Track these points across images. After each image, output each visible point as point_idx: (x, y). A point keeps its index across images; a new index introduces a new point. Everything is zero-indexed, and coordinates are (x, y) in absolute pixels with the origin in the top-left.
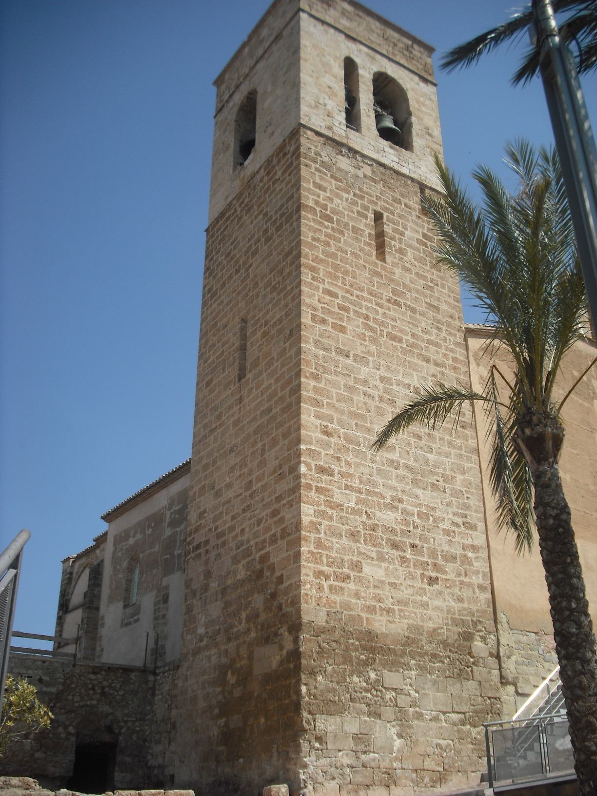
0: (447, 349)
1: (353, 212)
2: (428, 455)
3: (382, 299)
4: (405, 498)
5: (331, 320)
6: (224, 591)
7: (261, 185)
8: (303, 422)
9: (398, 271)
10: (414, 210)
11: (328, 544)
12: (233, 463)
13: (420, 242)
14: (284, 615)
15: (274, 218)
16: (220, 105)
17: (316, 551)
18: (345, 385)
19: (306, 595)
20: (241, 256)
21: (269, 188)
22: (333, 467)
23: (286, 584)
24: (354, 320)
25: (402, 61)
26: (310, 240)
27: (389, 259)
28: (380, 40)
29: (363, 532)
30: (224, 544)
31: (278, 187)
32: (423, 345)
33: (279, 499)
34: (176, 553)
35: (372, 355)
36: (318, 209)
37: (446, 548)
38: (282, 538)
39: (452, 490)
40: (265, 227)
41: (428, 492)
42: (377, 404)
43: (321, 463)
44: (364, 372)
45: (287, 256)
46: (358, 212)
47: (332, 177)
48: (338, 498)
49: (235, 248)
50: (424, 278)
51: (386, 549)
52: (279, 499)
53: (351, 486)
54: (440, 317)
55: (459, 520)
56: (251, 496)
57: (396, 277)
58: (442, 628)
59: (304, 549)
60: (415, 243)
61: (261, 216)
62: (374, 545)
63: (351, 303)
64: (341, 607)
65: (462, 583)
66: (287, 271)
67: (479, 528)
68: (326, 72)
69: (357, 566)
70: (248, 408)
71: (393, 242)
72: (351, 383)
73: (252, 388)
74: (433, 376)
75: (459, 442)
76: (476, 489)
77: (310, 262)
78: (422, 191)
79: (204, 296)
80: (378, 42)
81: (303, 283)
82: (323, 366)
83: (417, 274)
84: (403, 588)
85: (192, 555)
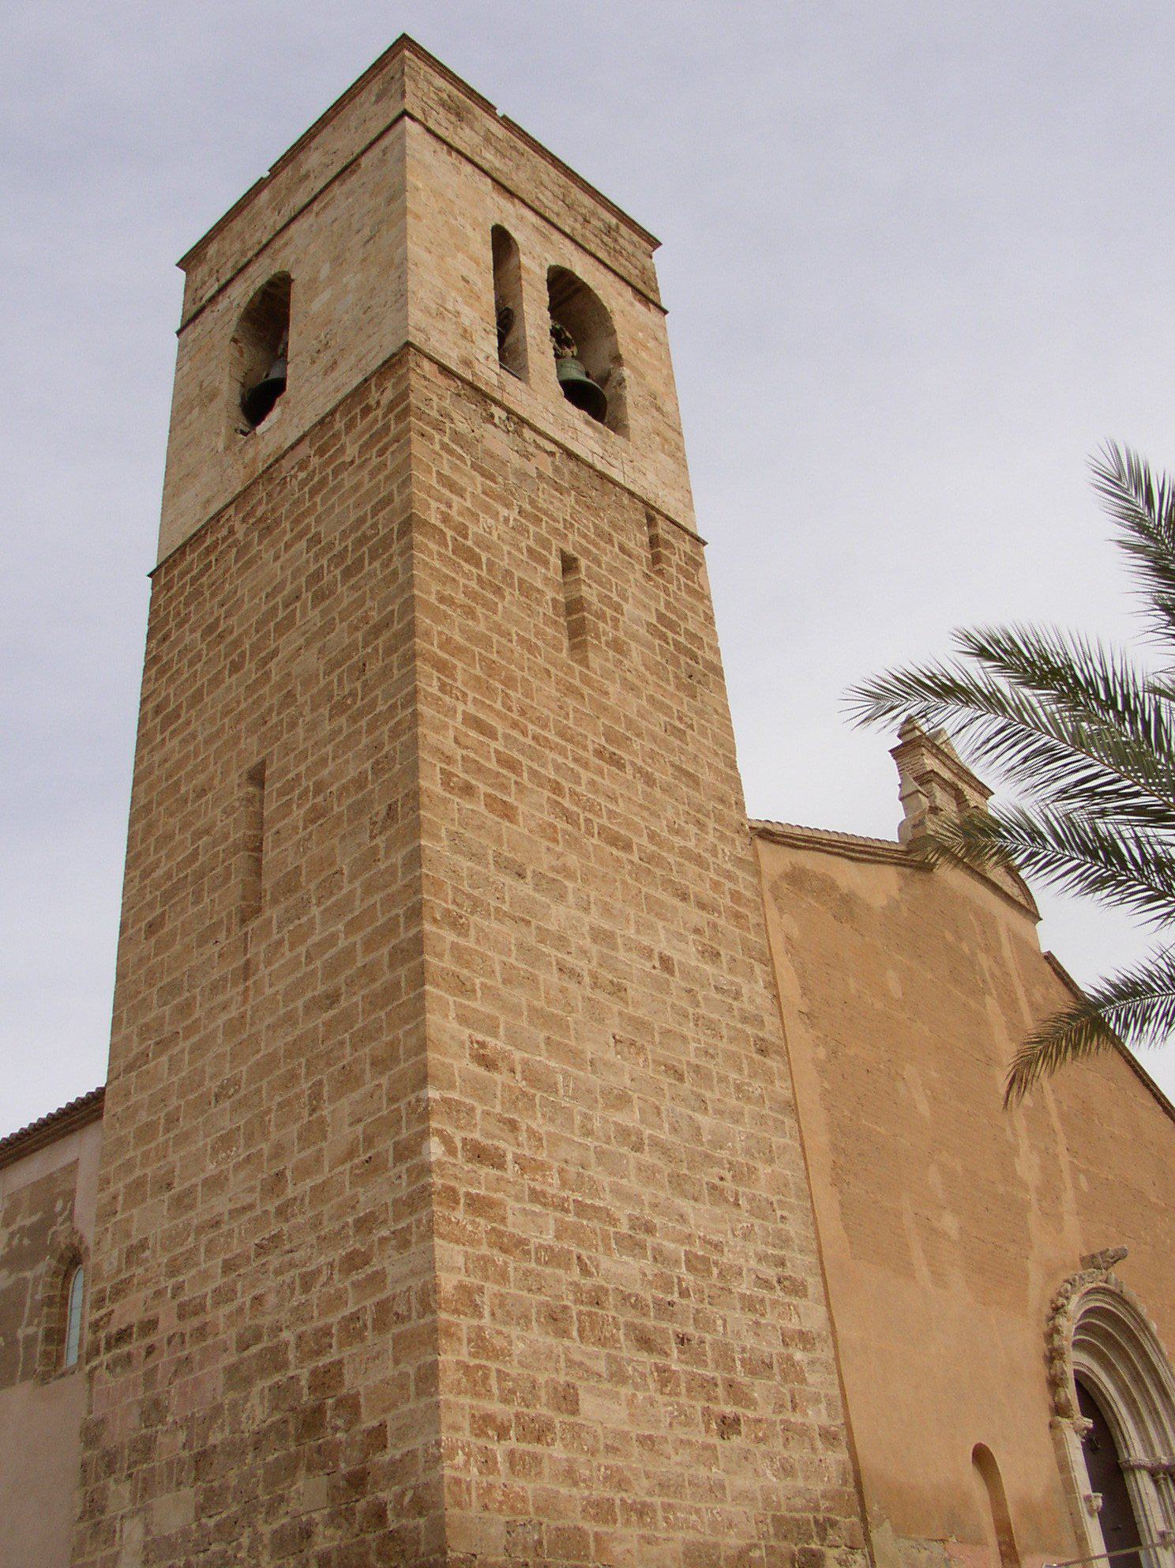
0: (719, 870)
1: (520, 550)
2: (698, 1116)
3: (585, 748)
4: (657, 1221)
5: (483, 789)
6: (202, 1460)
7: (302, 475)
8: (431, 1032)
9: (614, 688)
10: (639, 559)
11: (499, 1342)
12: (226, 1124)
13: (652, 629)
14: (392, 1536)
15: (338, 548)
16: (195, 309)
17: (473, 1362)
18: (520, 946)
19: (458, 1482)
20: (246, 632)
21: (324, 481)
22: (502, 1144)
23: (393, 1453)
24: (532, 791)
25: (601, 255)
26: (433, 599)
27: (595, 661)
28: (558, 207)
29: (574, 1310)
30: (201, 1332)
31: (348, 479)
32: (671, 859)
33: (365, 1224)
34: (21, 1334)
35: (571, 876)
36: (449, 533)
37: (750, 1342)
38: (380, 1325)
39: (752, 1199)
40: (313, 568)
41: (705, 1207)
42: (588, 992)
43: (477, 1135)
44: (558, 916)
45: (377, 631)
46: (530, 550)
47: (474, 466)
48: (515, 1225)
49: (228, 615)
50: (665, 709)
51: (627, 1350)
52: (365, 1224)
53: (544, 1194)
54: (699, 798)
55: (770, 1273)
56: (281, 1212)
57: (611, 702)
58: (756, 1546)
59: (446, 1358)
60: (643, 631)
61: (303, 544)
62: (601, 1342)
63: (522, 752)
64: (538, 1509)
65: (788, 1427)
66: (373, 668)
67: (810, 1290)
68: (458, 248)
69: (567, 1399)
70: (268, 991)
71: (601, 625)
72: (531, 940)
73: (280, 943)
74: (697, 931)
75: (757, 1086)
76: (798, 1197)
77: (435, 649)
78: (651, 521)
79: (142, 721)
80: (556, 208)
81: (421, 696)
82: (469, 896)
83: (651, 699)
84: (668, 1448)
85: (105, 1357)
